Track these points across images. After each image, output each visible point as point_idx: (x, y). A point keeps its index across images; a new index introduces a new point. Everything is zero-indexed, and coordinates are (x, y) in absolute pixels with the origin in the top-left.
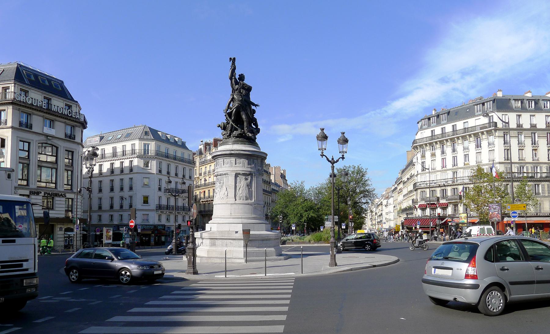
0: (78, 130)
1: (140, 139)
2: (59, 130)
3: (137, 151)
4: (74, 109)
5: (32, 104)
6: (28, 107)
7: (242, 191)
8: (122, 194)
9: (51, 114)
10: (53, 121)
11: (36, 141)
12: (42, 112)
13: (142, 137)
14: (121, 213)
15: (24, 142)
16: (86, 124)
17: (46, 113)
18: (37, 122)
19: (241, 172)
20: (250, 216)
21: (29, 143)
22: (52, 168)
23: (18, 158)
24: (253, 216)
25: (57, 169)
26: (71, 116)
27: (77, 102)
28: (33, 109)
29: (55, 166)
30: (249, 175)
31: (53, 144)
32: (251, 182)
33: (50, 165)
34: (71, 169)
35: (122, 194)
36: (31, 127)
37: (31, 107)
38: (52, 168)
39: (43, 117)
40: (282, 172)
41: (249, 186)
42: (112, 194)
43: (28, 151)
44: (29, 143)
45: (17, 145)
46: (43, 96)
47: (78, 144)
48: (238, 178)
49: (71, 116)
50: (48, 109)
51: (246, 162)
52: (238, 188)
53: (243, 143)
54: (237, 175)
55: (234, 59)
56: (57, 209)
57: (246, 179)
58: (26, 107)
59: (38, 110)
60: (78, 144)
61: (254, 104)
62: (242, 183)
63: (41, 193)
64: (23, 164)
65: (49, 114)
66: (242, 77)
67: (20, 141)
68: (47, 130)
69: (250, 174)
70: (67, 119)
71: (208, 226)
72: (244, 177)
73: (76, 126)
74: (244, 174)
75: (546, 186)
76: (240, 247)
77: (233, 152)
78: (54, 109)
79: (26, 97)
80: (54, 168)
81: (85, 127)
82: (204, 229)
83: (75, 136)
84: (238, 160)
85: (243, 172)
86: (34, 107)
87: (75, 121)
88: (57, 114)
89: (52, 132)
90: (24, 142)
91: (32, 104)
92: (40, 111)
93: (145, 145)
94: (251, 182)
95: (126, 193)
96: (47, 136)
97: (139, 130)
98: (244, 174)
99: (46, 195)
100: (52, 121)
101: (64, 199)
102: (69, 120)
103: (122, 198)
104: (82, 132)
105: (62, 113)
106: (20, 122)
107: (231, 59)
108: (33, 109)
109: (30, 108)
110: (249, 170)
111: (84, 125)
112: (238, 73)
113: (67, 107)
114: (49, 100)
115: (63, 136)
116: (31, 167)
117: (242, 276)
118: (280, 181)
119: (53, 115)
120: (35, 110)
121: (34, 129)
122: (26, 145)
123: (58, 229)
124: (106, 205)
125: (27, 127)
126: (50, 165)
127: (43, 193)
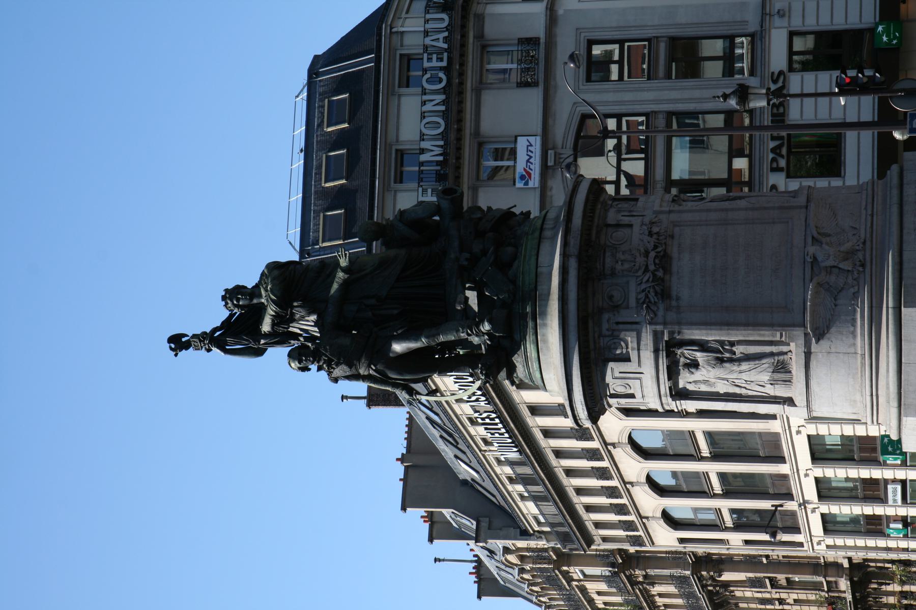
21: (591, 43)
24: (861, 343)
41: (723, 356)
49: (445, 69)
57: (694, 365)
65: (458, 168)
70: (461, 83)
85: (663, 376)
87: (463, 45)
88: (452, 136)
94: (703, 346)
110: (647, 356)
115: (534, 97)
119: (459, 149)
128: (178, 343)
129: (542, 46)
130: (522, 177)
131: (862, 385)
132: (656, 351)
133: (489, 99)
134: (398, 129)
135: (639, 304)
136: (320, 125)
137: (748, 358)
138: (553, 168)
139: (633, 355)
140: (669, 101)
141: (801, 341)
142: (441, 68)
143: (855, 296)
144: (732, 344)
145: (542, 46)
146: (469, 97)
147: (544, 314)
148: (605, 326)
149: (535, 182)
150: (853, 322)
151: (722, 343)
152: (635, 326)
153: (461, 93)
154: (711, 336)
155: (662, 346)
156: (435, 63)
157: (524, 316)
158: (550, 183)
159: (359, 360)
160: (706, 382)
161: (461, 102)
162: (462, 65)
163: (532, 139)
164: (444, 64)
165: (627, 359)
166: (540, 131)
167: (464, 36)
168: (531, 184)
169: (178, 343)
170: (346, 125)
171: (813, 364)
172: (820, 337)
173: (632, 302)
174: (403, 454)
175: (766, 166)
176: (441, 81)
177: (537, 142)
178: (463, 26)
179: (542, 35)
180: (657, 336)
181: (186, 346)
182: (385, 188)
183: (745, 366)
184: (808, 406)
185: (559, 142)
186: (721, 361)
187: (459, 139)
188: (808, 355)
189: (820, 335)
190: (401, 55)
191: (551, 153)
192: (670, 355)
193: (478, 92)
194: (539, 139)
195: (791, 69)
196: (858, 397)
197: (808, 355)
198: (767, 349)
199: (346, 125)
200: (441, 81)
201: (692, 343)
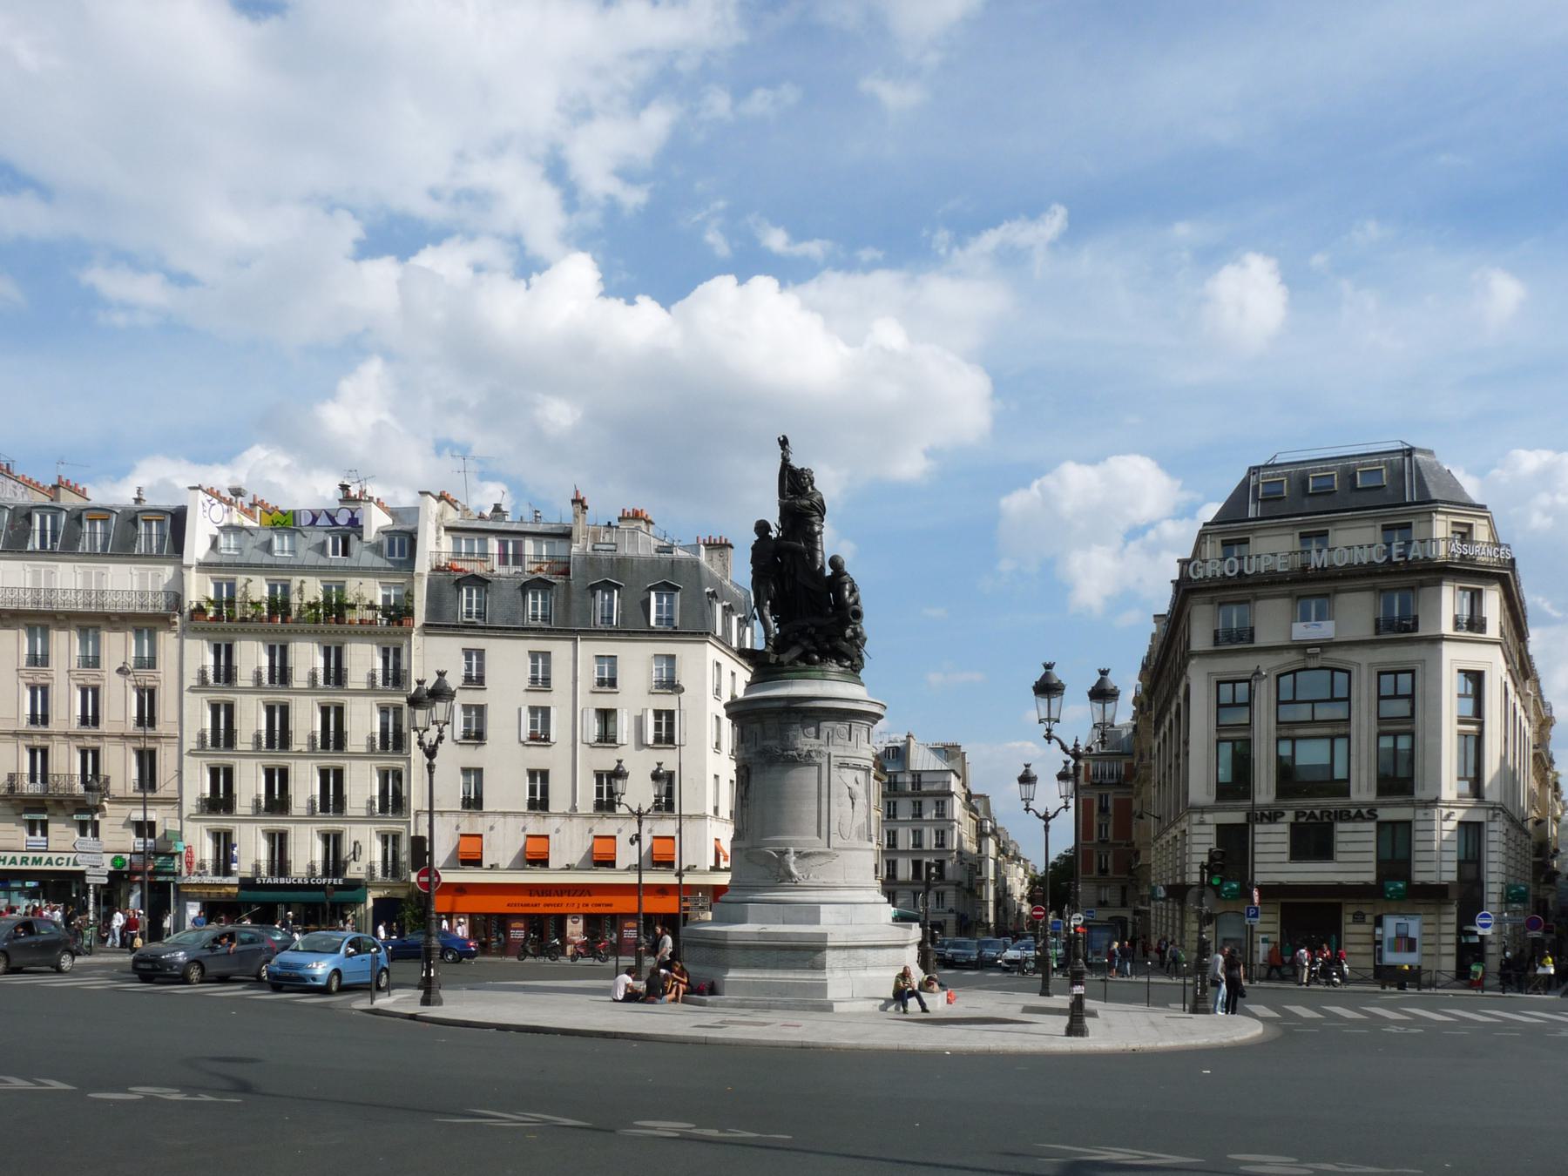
4: (1481, 533)
6: (1233, 587)
11: (1370, 665)
22: (1332, 738)
25: (1348, 736)
33: (1326, 731)
38: (1332, 738)
39: (1289, 595)
46: (1379, 525)
56: (1339, 857)
64: (1233, 741)
68: (1303, 631)
75: (510, 545)
83: (1416, 618)
96: (1302, 647)
101: (1372, 826)
117: (772, 928)
121: (1261, 640)
123: (1349, 919)
126: (1326, 731)
128: (784, 443)
169: (784, 443)
173: (766, 743)
181: (783, 448)
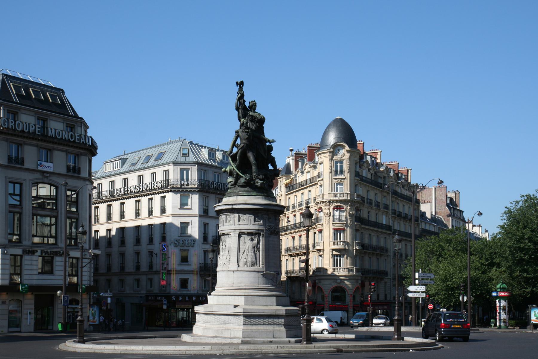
0: (84, 160)
1: (175, 163)
2: (59, 162)
3: (171, 182)
5: (22, 131)
7: (248, 256)
8: (151, 247)
9: (47, 142)
10: (50, 150)
11: (30, 180)
12: (36, 139)
13: (178, 160)
14: (150, 277)
15: (14, 183)
16: (96, 148)
17: (42, 140)
18: (30, 154)
19: (246, 231)
20: (256, 285)
21: (21, 184)
23: (8, 207)
24: (262, 286)
26: (74, 141)
27: (82, 118)
28: (24, 137)
29: (55, 214)
30: (256, 234)
31: (51, 182)
32: (258, 243)
34: (75, 216)
35: (151, 247)
36: (23, 163)
37: (23, 134)
40: (452, 195)
41: (256, 248)
42: (137, 248)
43: (20, 195)
44: (21, 184)
45: (7, 188)
47: (85, 179)
48: (241, 238)
49: (74, 141)
50: (43, 135)
51: (252, 217)
52: (241, 251)
53: (248, 194)
54: (240, 235)
55: (242, 83)
57: (252, 240)
58: (15, 135)
59: (30, 138)
60: (85, 179)
61: (269, 141)
62: (247, 243)
63: (37, 251)
65: (45, 141)
66: (253, 106)
67: (10, 182)
69: (258, 234)
70: (69, 146)
71: (210, 298)
72: (249, 237)
73: (81, 154)
74: (249, 234)
76: (239, 324)
77: (235, 207)
78: (51, 133)
79: (15, 121)
80: (53, 217)
81: (94, 154)
82: (205, 302)
83: (79, 168)
84: (243, 217)
85: (249, 231)
86: (25, 135)
87: (80, 148)
88: (55, 140)
89: (48, 167)
90: (14, 183)
91: (22, 131)
92: (33, 139)
93: (182, 170)
94: (258, 243)
95: (157, 247)
96: (43, 172)
97: (172, 152)
98: (249, 234)
99: (43, 254)
100: (49, 150)
102: (72, 146)
103: (151, 253)
104: (90, 161)
105: (62, 138)
106: (9, 156)
107: (237, 83)
108: (24, 137)
109: (21, 136)
110: (256, 227)
111: (91, 150)
112: (248, 100)
113: (69, 129)
114: (45, 121)
115: (63, 171)
116: (24, 217)
118: (444, 214)
119: (50, 142)
120: (27, 138)
121: (27, 165)
122: (17, 186)
124: (130, 267)
125: (17, 163)
127: (39, 251)
128: (241, 84)
129: (77, 175)
130: (41, 164)
131: (248, 286)
132: (258, 230)
133: (63, 154)
134: (25, 114)
135: (270, 226)
136: (32, 87)
137: (255, 255)
138: (43, 175)
139: (257, 223)
140: (61, 217)
141: (262, 270)
142: (75, 140)
143: (272, 285)
144: (259, 251)
145: (77, 175)
146: (34, 142)
147: (265, 199)
148: (265, 216)
149: (40, 168)
150: (266, 284)
151: (259, 248)
152: (264, 225)
153: (67, 145)
154: (262, 245)
155: (259, 232)
156: (77, 137)
157: (262, 193)
158: (39, 174)
159: (248, 141)
160: (245, 243)
161: (64, 145)
162: (75, 147)
163: (52, 168)
164: (76, 141)
165: (255, 221)
166: (55, 172)
167: (82, 149)
168: (39, 167)
169: (241, 84)
170: (34, 97)
171: (255, 273)
172: (263, 275)
173: (270, 224)
174: (417, 185)
175: (43, 249)
176: (72, 139)
177: (51, 170)
178: (85, 149)
179: (81, 175)
180: (262, 231)
182: (36, 113)
183: (253, 254)
184: (238, 271)
185: (51, 178)
186: (254, 248)
187: (53, 143)
188: (258, 272)
189: (264, 275)
190: (75, 125)
191: (48, 175)
192: (256, 234)
193: (37, 146)
194: (52, 171)
195: (21, 256)
196: (243, 285)
197: (258, 272)
198: (258, 261)
199: (34, 97)
200: (72, 139)
201: (259, 240)
